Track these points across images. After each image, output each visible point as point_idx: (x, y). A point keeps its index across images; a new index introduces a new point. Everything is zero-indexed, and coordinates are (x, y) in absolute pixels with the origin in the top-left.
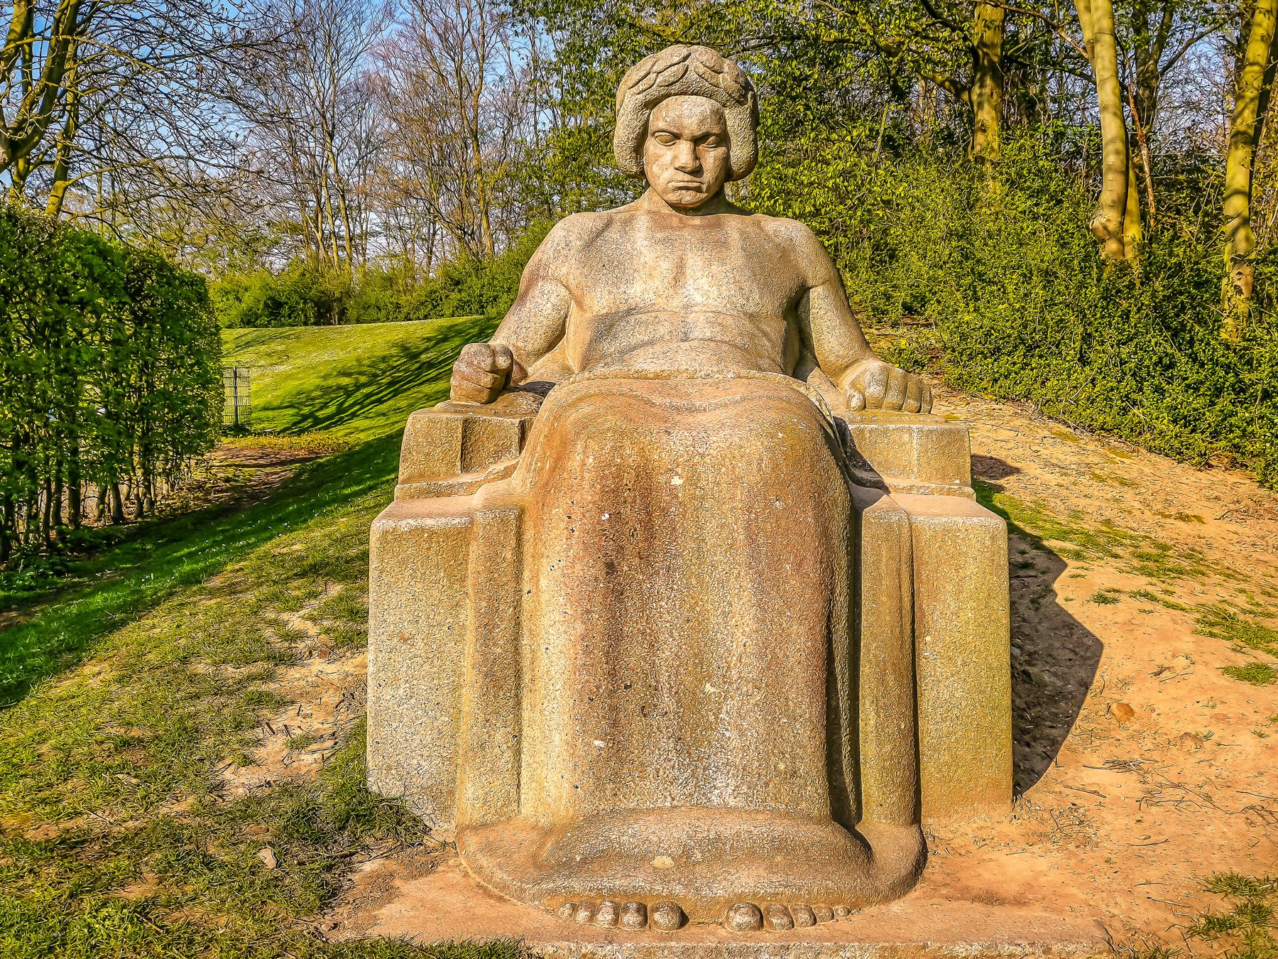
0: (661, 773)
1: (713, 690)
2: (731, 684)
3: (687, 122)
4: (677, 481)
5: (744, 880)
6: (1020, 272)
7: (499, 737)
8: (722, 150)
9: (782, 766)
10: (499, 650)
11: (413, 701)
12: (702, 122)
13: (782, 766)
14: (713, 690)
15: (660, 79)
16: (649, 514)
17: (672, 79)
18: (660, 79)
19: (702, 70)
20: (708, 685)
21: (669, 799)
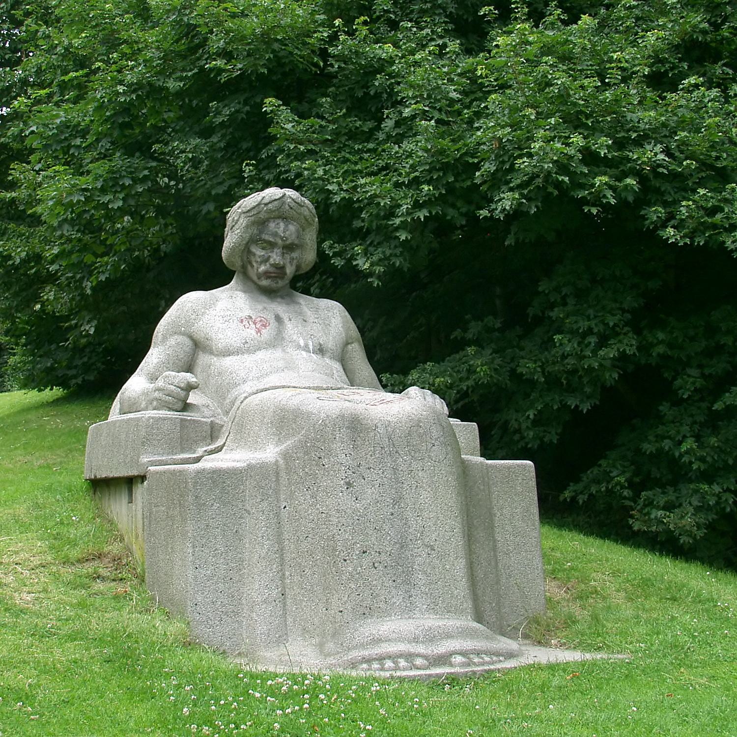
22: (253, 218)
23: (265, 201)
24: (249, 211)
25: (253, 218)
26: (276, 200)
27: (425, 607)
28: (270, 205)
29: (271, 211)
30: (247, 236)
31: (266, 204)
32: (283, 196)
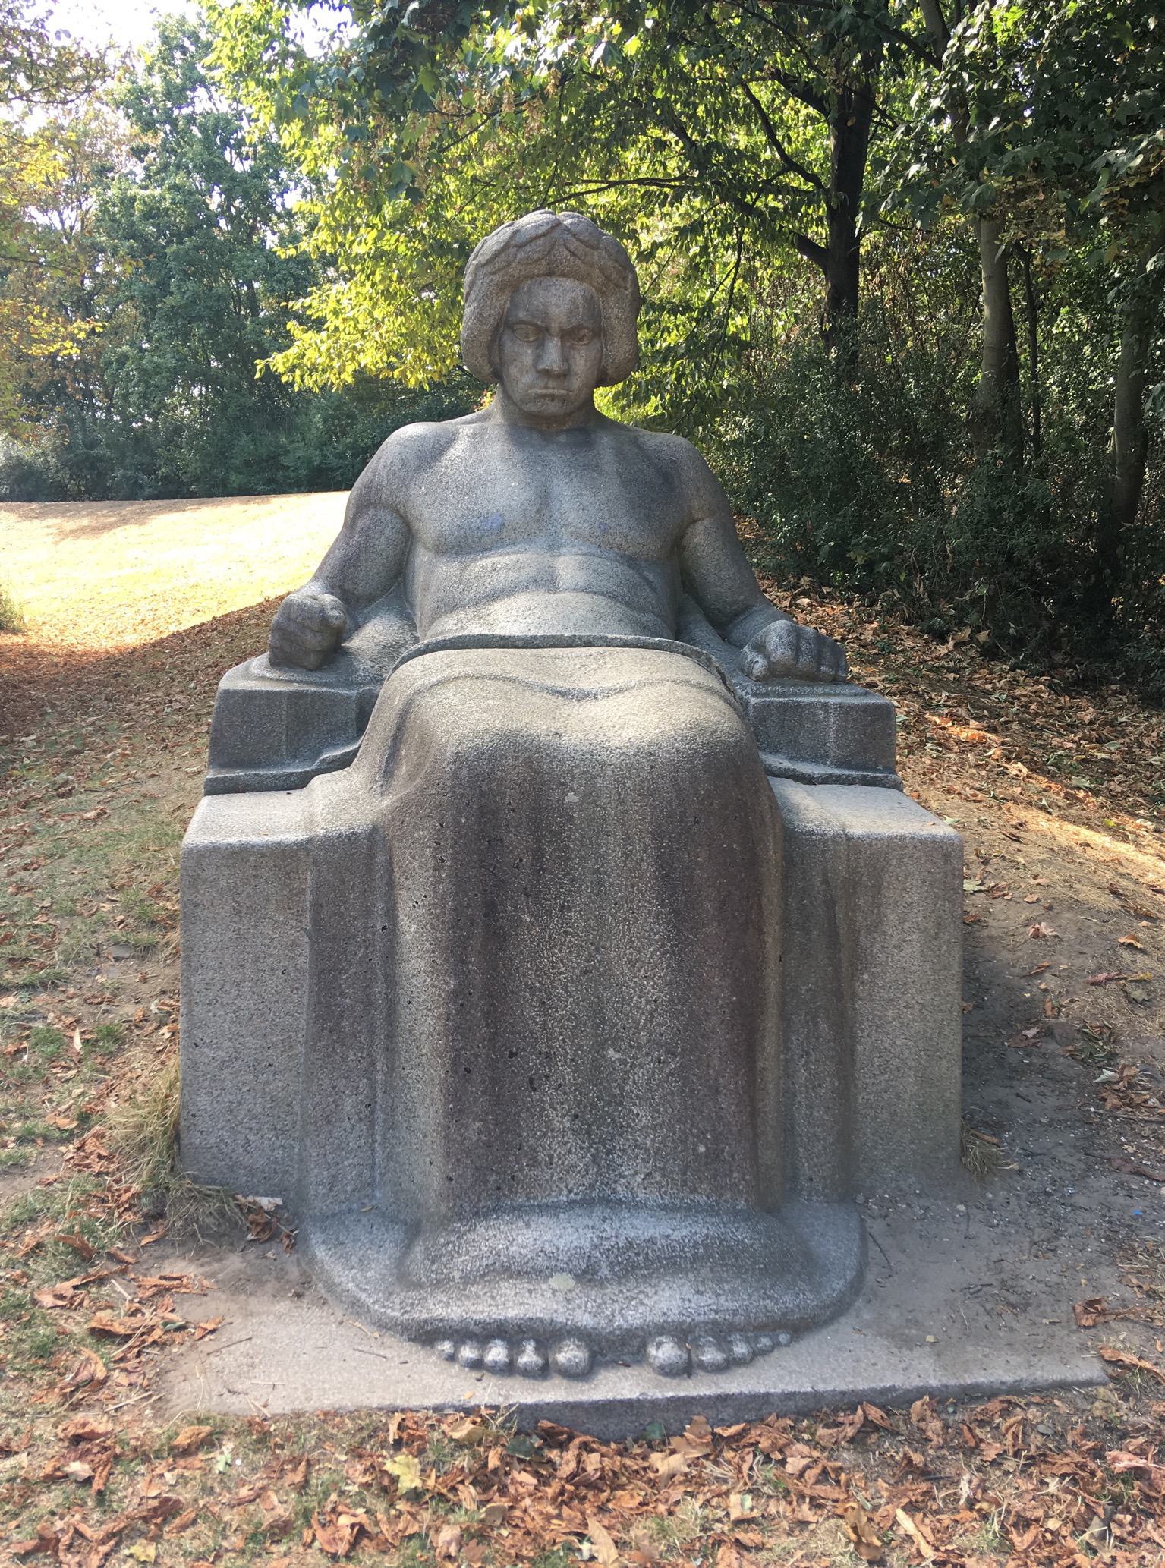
0: (555, 1160)
1: (617, 1056)
2: (639, 1048)
3: (554, 312)
4: (572, 798)
5: (664, 1306)
6: (1065, 1463)
7: (348, 1105)
8: (596, 345)
9: (702, 1149)
10: (348, 1001)
11: (237, 1064)
12: (571, 313)
13: (702, 1149)
14: (617, 1056)
15: (521, 255)
16: (538, 841)
17: (536, 256)
18: (521, 255)
19: (574, 244)
20: (611, 1051)
21: (565, 1192)
22: (497, 278)
23: (519, 240)
24: (489, 261)
25: (497, 278)
26: (538, 237)
27: (639, 1178)
28: (528, 248)
29: (530, 262)
30: (492, 314)
31: (520, 246)
32: (553, 228)
